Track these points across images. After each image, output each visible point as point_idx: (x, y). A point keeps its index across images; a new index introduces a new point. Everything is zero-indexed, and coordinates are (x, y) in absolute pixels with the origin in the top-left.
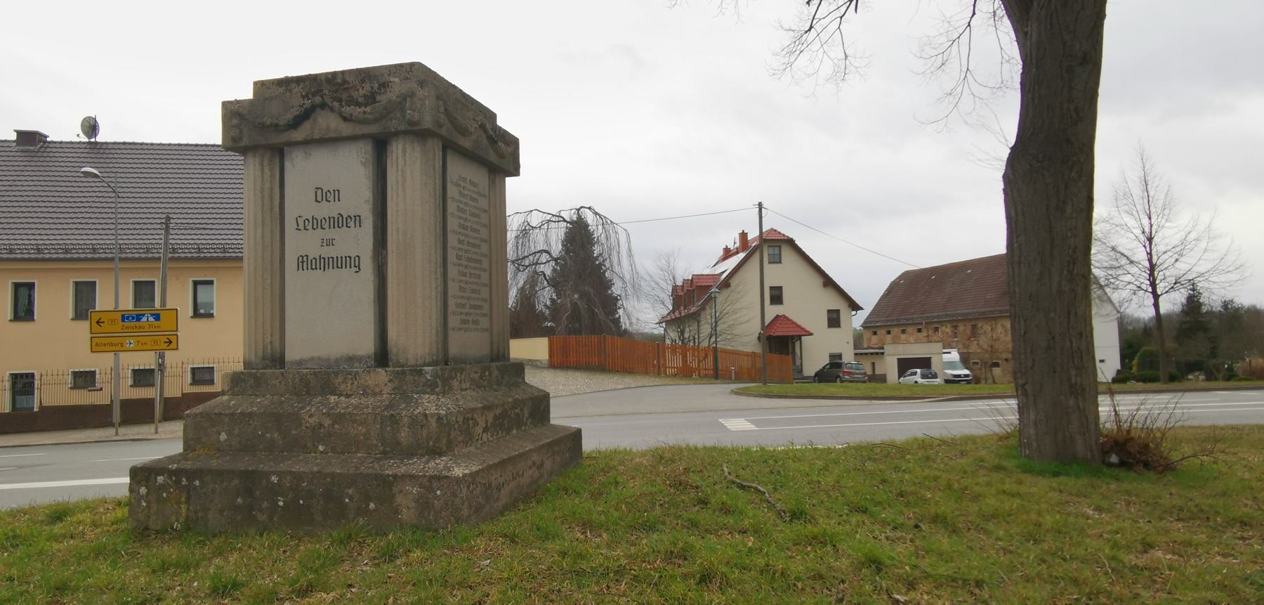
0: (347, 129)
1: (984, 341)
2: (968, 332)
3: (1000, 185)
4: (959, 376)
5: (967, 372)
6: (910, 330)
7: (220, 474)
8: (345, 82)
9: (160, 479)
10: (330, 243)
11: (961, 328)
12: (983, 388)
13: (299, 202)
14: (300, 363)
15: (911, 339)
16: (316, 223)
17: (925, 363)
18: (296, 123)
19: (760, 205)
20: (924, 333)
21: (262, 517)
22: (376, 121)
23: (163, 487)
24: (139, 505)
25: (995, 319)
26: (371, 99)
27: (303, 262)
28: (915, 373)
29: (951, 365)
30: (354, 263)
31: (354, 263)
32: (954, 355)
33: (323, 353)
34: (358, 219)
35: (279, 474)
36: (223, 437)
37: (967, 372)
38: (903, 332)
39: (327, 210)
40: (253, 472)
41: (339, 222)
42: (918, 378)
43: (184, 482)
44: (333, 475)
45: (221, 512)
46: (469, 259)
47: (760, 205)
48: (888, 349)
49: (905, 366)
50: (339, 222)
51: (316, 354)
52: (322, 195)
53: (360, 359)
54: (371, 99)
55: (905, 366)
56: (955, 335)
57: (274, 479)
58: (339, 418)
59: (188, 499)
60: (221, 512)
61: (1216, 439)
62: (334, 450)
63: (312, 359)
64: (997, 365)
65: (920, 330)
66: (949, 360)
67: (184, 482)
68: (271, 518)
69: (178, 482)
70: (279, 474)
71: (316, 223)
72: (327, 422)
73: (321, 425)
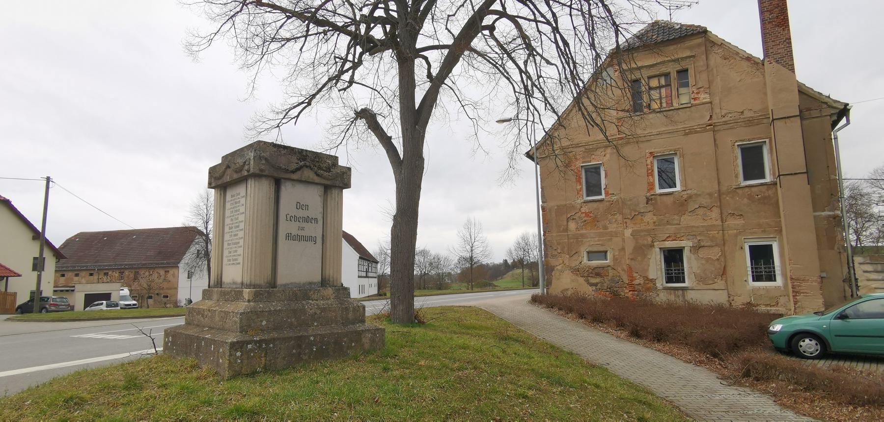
0: (317, 179)
1: (144, 283)
2: (132, 275)
3: (390, 224)
4: (129, 305)
5: (135, 302)
6: (83, 274)
7: (284, 339)
8: (307, 155)
9: (250, 346)
10: (303, 229)
11: (127, 273)
12: (143, 311)
13: (287, 205)
14: (285, 285)
15: (83, 281)
16: (296, 219)
17: (107, 297)
18: (293, 172)
19: (48, 180)
20: (95, 277)
21: (305, 357)
22: (328, 179)
23: (251, 351)
24: (236, 362)
25: (154, 268)
26: (328, 169)
27: (289, 236)
28: (102, 304)
29: (123, 298)
30: (313, 239)
31: (313, 239)
32: (126, 292)
33: (297, 280)
34: (316, 220)
35: (314, 336)
36: (264, 323)
37: (135, 302)
38: (77, 275)
39: (301, 213)
40: (301, 336)
41: (307, 220)
42: (103, 307)
43: (264, 346)
44: (338, 333)
45: (284, 358)
47: (48, 180)
48: (78, 287)
49: (91, 299)
50: (307, 220)
51: (293, 281)
52: (300, 206)
53: (315, 283)
54: (328, 169)
55: (91, 299)
56: (122, 278)
57: (312, 338)
58: (323, 310)
59: (266, 354)
60: (284, 358)
61: (444, 311)
62: (321, 324)
63: (291, 283)
64: (151, 297)
65: (91, 275)
66: (123, 293)
67: (264, 346)
68: (309, 357)
69: (260, 346)
70: (314, 336)
71: (296, 219)
72: (318, 312)
73: (316, 313)
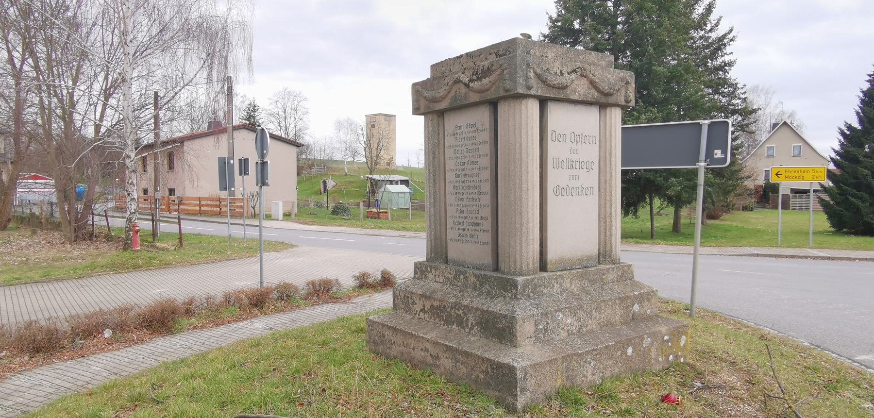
46: (466, 188)
